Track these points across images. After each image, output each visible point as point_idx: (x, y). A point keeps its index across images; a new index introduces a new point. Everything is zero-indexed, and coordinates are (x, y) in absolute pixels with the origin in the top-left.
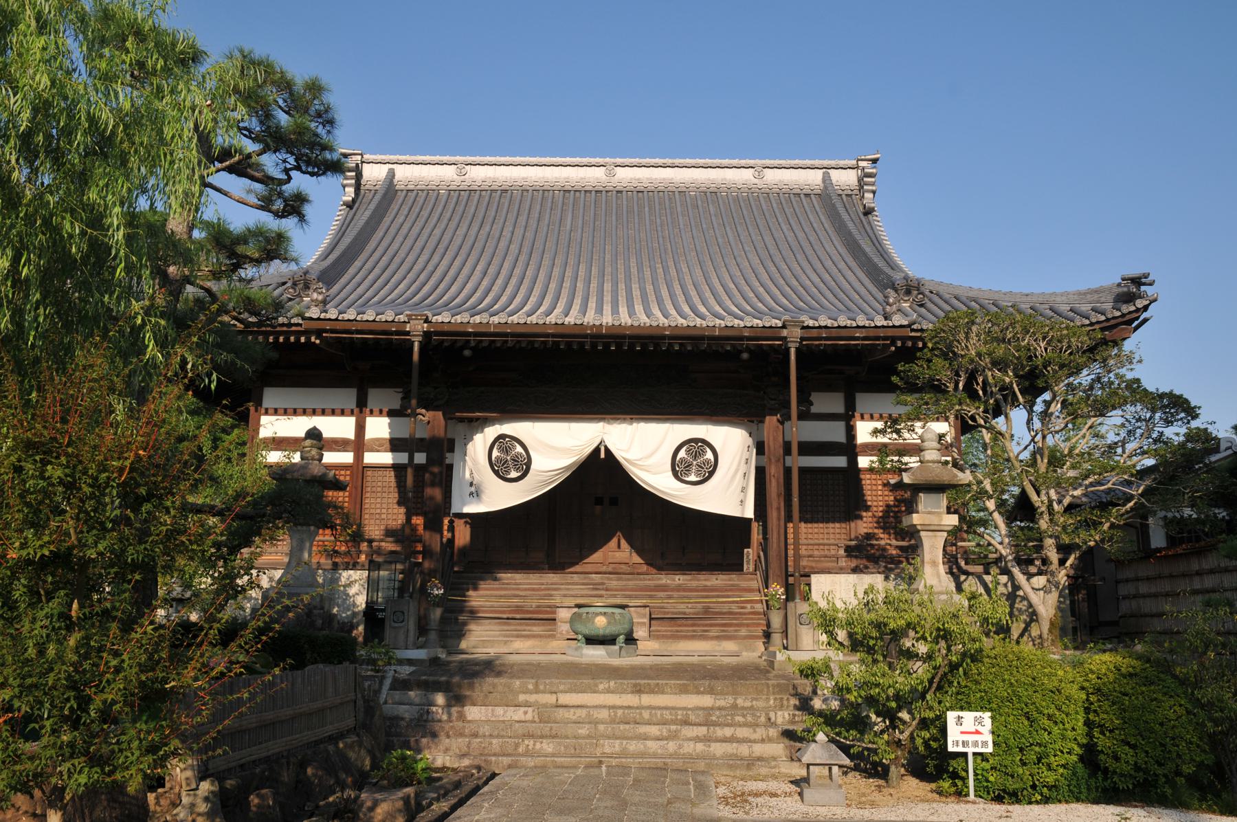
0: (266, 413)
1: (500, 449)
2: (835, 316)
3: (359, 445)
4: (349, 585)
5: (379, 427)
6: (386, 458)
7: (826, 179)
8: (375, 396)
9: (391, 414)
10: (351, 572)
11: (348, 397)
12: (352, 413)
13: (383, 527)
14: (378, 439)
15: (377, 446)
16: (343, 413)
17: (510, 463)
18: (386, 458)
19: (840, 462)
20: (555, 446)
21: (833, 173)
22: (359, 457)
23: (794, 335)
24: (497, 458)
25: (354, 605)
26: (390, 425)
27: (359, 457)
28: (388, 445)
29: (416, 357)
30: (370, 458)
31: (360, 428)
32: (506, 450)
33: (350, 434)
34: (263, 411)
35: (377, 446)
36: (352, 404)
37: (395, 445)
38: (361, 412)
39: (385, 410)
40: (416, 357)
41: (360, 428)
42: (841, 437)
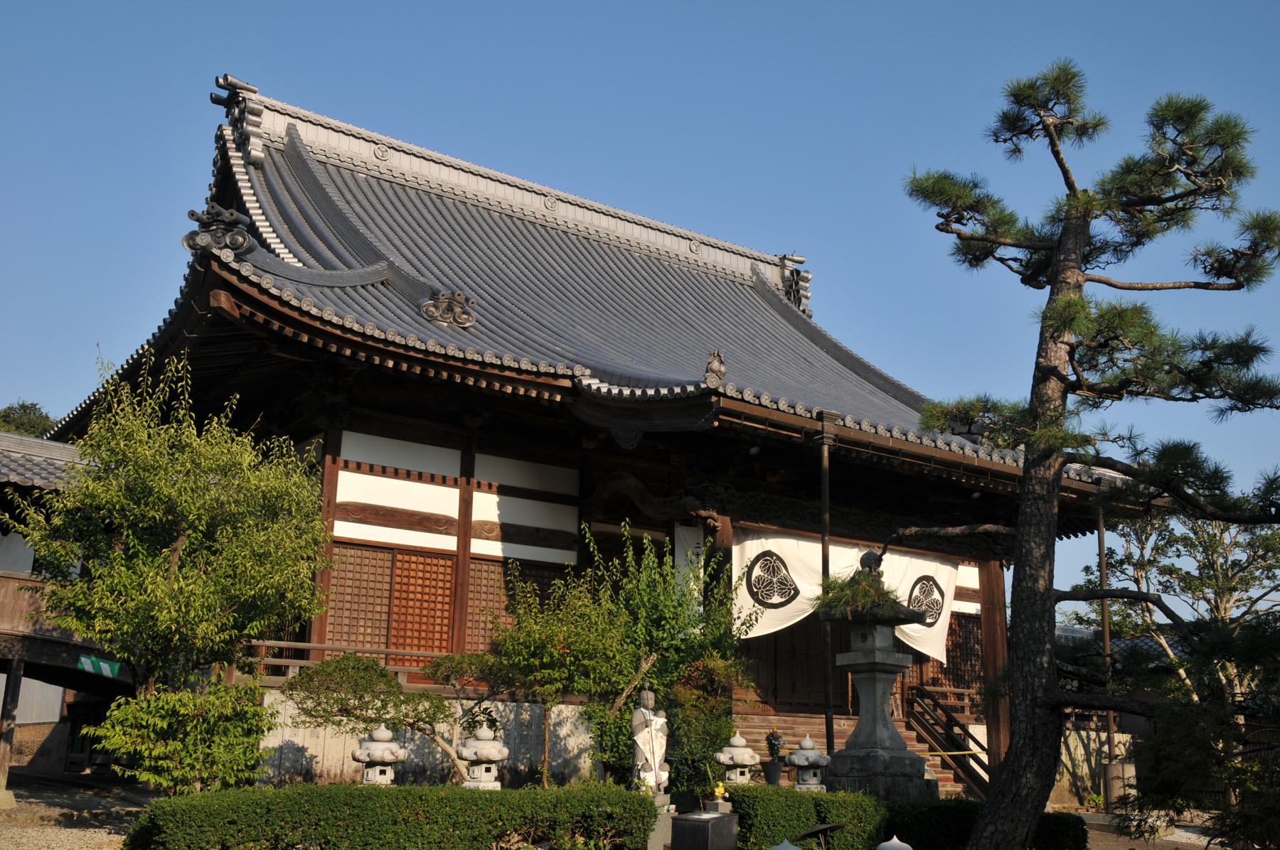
0: (346, 467)
1: (763, 567)
2: (463, 346)
3: (464, 527)
4: (559, 724)
5: (487, 507)
6: (494, 548)
7: (291, 130)
8: (485, 465)
9: (503, 491)
10: (562, 707)
11: (449, 461)
12: (455, 484)
13: (488, 640)
14: (486, 523)
15: (484, 531)
16: (444, 482)
17: (773, 584)
18: (494, 548)
19: (449, 543)
20: (811, 565)
21: (301, 126)
22: (464, 544)
23: (830, 428)
24: (758, 578)
25: (566, 750)
26: (500, 505)
27: (464, 544)
28: (497, 532)
29: (826, 462)
30: (479, 546)
31: (466, 504)
32: (772, 570)
33: (454, 513)
34: (342, 464)
35: (484, 531)
36: (454, 471)
37: (508, 533)
38: (468, 483)
39: (495, 484)
40: (826, 462)
41: (466, 504)
42: (454, 513)
